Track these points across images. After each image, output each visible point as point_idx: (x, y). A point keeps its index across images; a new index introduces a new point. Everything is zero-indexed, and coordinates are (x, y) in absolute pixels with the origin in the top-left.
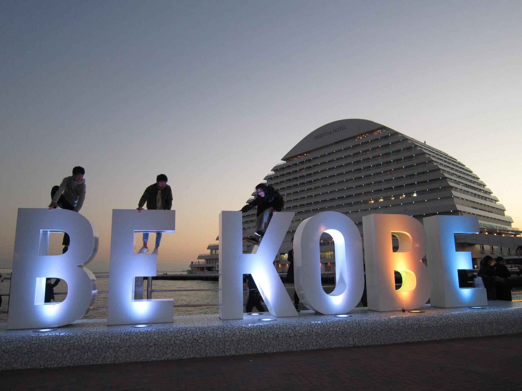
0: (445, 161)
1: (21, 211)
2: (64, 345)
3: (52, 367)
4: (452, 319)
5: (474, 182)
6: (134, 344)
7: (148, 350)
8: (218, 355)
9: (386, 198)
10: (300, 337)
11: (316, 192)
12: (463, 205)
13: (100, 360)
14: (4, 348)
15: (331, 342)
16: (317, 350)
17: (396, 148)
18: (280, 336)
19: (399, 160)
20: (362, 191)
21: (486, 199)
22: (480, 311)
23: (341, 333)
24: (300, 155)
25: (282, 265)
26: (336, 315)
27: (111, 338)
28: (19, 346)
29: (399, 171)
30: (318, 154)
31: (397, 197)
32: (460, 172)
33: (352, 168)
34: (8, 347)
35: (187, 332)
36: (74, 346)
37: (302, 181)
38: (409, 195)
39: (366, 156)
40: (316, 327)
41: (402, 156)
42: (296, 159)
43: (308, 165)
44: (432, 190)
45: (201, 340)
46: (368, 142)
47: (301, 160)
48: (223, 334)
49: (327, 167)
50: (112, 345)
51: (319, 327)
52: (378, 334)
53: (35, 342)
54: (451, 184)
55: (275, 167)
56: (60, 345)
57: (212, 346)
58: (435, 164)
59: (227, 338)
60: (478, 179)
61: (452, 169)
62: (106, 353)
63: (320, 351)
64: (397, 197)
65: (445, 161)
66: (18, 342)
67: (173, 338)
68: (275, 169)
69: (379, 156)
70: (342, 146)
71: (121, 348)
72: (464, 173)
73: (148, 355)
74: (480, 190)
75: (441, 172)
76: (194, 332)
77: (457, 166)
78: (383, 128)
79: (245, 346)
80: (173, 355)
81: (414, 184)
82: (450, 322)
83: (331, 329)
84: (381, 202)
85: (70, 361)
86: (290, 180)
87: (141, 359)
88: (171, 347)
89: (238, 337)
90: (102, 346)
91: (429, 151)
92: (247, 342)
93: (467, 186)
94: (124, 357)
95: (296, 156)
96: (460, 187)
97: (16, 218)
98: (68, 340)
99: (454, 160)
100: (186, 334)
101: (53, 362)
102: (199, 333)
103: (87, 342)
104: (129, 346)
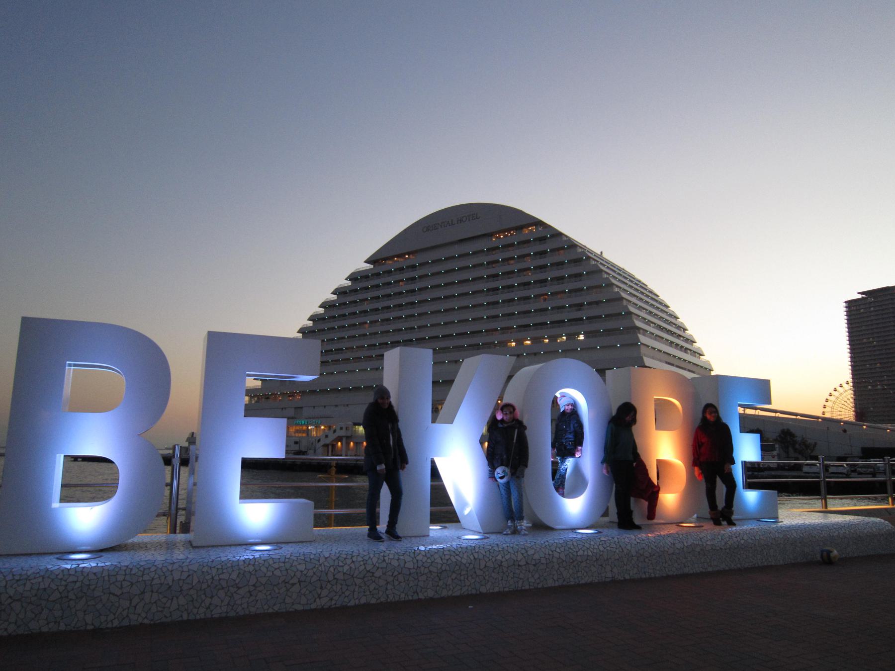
0: (631, 287)
1: (27, 323)
2: (132, 584)
3: (110, 625)
4: (745, 538)
5: (671, 323)
6: (263, 580)
7: (288, 590)
8: (407, 599)
9: (536, 340)
10: (534, 565)
11: (422, 322)
12: (653, 358)
13: (202, 610)
14: (11, 592)
15: (579, 574)
16: (560, 587)
17: (557, 258)
18: (505, 564)
19: (561, 279)
20: (498, 325)
21: (686, 350)
22: (774, 526)
23: (594, 559)
24: (398, 256)
25: (356, 444)
26: (573, 530)
27: (220, 572)
28: (42, 587)
29: (559, 296)
30: (429, 257)
31: (553, 338)
32: (652, 305)
33: (484, 286)
34: (20, 589)
35: (354, 559)
36: (151, 586)
37: (386, 303)
38: (572, 336)
39: (507, 268)
40: (558, 550)
41: (566, 272)
42: (390, 262)
43: (411, 274)
44: (609, 332)
45: (377, 574)
46: (512, 245)
47: (398, 266)
48: (415, 561)
49: (442, 281)
50: (224, 584)
51: (562, 549)
52: (647, 560)
53: (75, 579)
54: (638, 324)
55: (352, 274)
56: (125, 584)
57: (396, 583)
58: (616, 290)
59: (422, 568)
60: (677, 318)
61: (641, 299)
62: (212, 597)
63: (564, 589)
64: (553, 338)
65: (631, 287)
66: (40, 579)
67: (332, 569)
68: (353, 278)
69: (529, 269)
70: (470, 248)
71: (239, 588)
72: (658, 308)
73: (288, 600)
74: (680, 336)
75: (625, 303)
76: (367, 558)
77: (647, 296)
78: (539, 223)
79: (450, 582)
80: (331, 599)
81: (582, 319)
82: (742, 542)
83: (581, 553)
84: (528, 346)
85: (143, 615)
86: (377, 298)
87: (276, 608)
88: (329, 586)
89: (439, 566)
90: (204, 586)
91: (608, 268)
92: (454, 576)
93: (660, 328)
94: (245, 606)
95: (391, 258)
96: (650, 329)
97: (18, 334)
98: (140, 574)
99: (644, 287)
100: (353, 562)
101: (111, 617)
102: (375, 560)
103: (176, 578)
104: (254, 585)
